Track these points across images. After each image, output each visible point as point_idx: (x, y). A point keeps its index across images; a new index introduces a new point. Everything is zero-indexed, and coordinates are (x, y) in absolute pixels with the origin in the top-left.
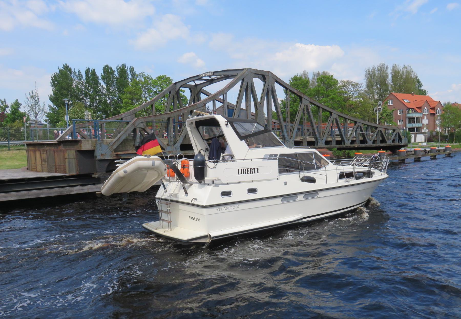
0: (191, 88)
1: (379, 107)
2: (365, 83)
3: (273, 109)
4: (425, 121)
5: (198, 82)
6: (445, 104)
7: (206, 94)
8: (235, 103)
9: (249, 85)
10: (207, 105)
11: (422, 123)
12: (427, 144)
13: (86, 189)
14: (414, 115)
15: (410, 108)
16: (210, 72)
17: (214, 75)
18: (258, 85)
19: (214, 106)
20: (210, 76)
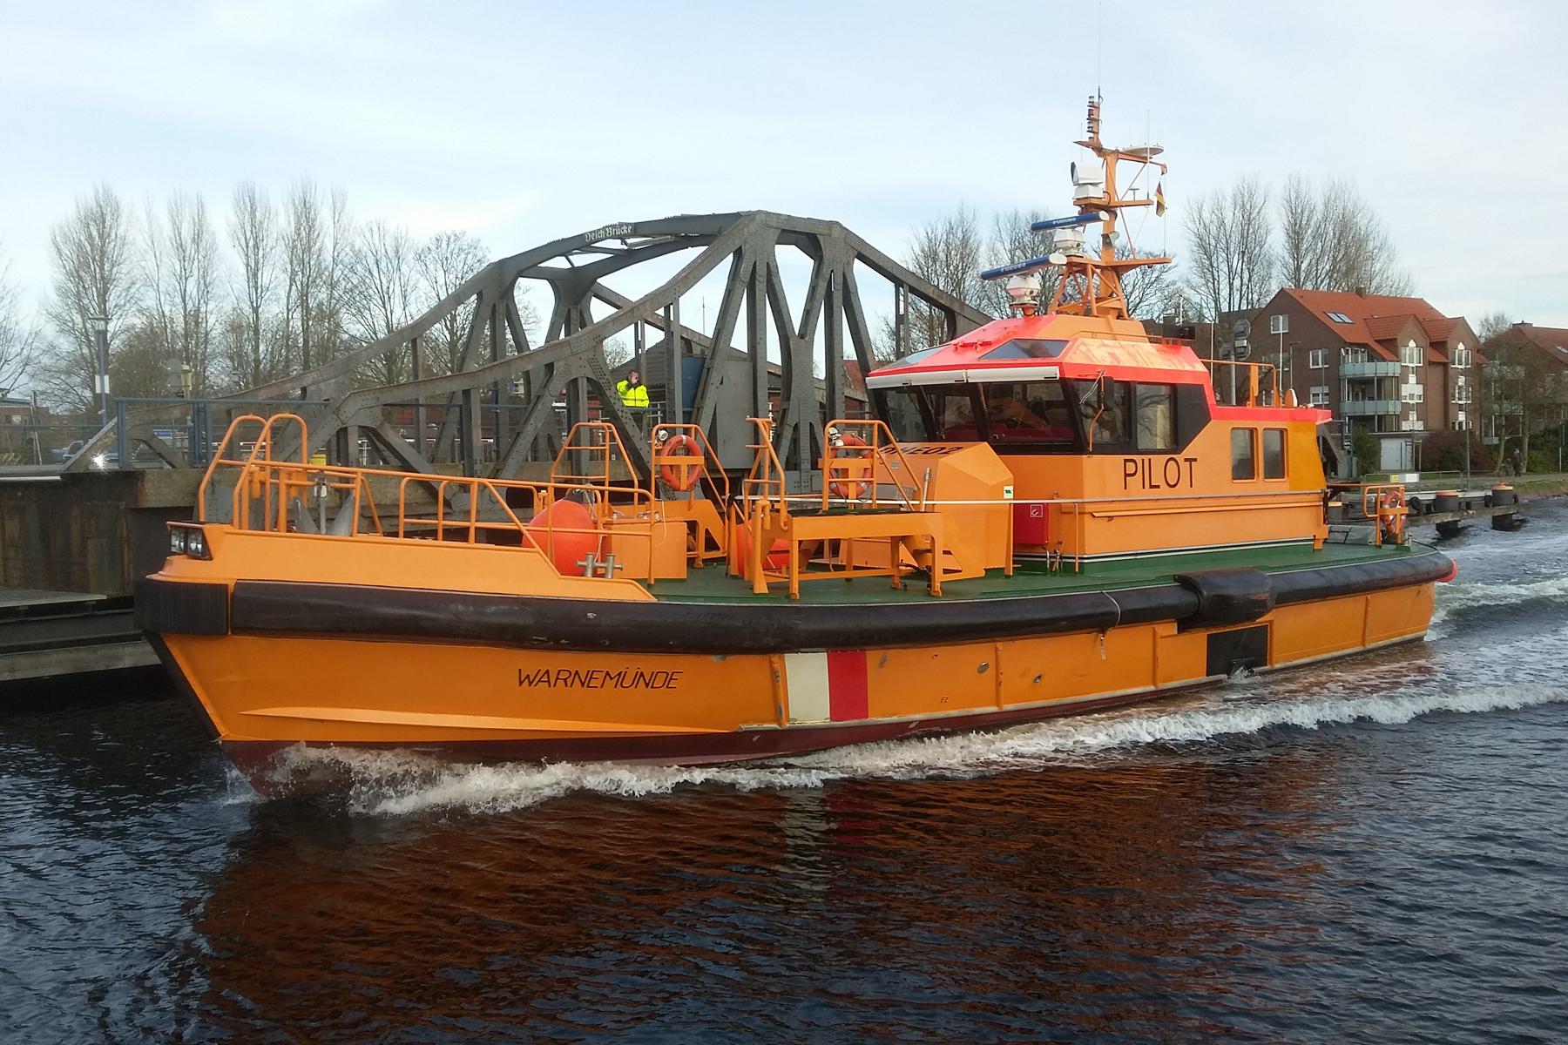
0: (554, 278)
1: (1238, 344)
2: (1187, 255)
3: (849, 351)
4: (1412, 389)
5: (581, 260)
6: (1485, 323)
7: (609, 298)
8: (710, 333)
9: (761, 271)
10: (609, 344)
11: (1398, 397)
12: (1421, 478)
13: (1525, 591)
14: (1369, 369)
15: (1351, 345)
16: (621, 225)
17: (634, 234)
18: (794, 269)
19: (639, 344)
20: (622, 238)
